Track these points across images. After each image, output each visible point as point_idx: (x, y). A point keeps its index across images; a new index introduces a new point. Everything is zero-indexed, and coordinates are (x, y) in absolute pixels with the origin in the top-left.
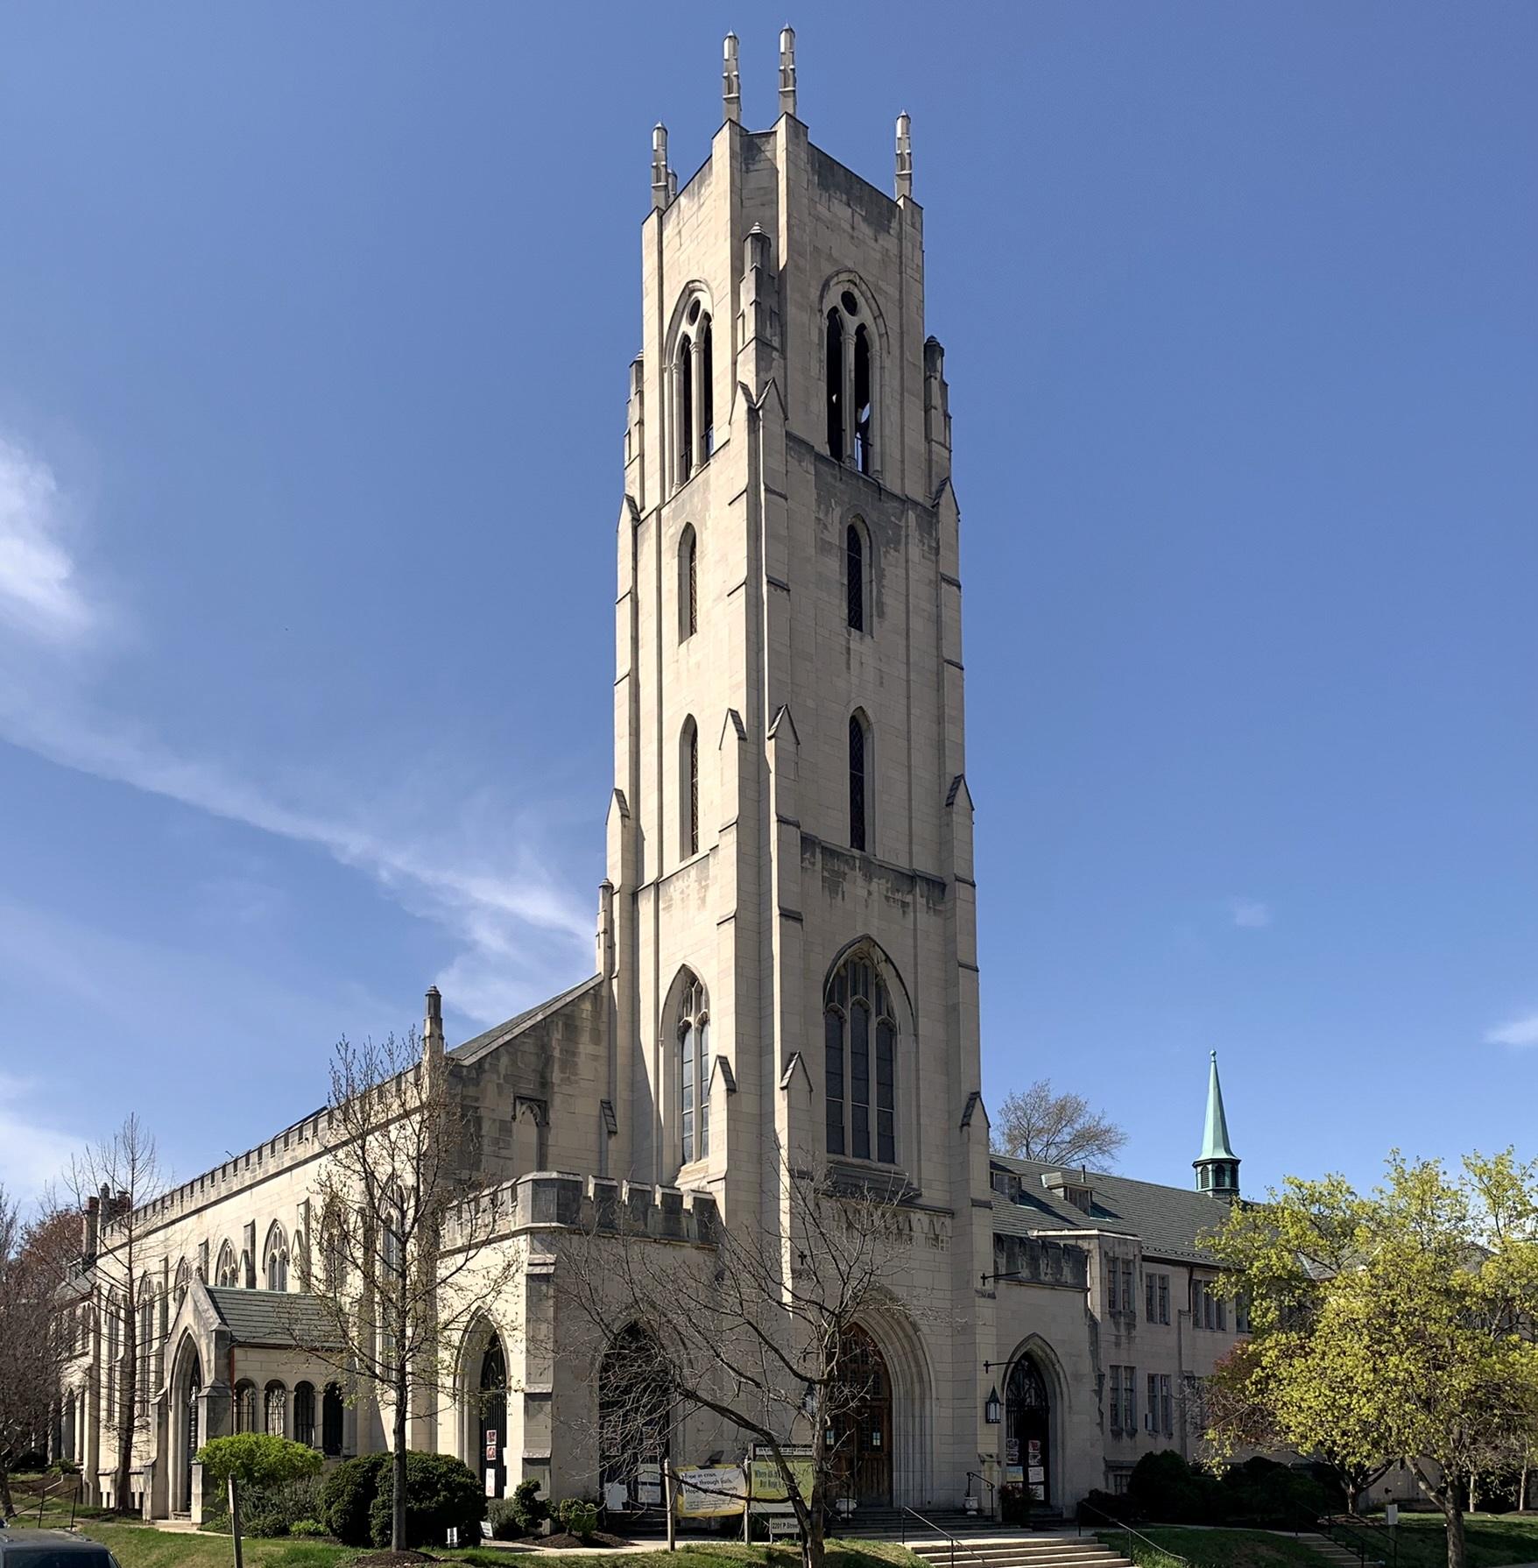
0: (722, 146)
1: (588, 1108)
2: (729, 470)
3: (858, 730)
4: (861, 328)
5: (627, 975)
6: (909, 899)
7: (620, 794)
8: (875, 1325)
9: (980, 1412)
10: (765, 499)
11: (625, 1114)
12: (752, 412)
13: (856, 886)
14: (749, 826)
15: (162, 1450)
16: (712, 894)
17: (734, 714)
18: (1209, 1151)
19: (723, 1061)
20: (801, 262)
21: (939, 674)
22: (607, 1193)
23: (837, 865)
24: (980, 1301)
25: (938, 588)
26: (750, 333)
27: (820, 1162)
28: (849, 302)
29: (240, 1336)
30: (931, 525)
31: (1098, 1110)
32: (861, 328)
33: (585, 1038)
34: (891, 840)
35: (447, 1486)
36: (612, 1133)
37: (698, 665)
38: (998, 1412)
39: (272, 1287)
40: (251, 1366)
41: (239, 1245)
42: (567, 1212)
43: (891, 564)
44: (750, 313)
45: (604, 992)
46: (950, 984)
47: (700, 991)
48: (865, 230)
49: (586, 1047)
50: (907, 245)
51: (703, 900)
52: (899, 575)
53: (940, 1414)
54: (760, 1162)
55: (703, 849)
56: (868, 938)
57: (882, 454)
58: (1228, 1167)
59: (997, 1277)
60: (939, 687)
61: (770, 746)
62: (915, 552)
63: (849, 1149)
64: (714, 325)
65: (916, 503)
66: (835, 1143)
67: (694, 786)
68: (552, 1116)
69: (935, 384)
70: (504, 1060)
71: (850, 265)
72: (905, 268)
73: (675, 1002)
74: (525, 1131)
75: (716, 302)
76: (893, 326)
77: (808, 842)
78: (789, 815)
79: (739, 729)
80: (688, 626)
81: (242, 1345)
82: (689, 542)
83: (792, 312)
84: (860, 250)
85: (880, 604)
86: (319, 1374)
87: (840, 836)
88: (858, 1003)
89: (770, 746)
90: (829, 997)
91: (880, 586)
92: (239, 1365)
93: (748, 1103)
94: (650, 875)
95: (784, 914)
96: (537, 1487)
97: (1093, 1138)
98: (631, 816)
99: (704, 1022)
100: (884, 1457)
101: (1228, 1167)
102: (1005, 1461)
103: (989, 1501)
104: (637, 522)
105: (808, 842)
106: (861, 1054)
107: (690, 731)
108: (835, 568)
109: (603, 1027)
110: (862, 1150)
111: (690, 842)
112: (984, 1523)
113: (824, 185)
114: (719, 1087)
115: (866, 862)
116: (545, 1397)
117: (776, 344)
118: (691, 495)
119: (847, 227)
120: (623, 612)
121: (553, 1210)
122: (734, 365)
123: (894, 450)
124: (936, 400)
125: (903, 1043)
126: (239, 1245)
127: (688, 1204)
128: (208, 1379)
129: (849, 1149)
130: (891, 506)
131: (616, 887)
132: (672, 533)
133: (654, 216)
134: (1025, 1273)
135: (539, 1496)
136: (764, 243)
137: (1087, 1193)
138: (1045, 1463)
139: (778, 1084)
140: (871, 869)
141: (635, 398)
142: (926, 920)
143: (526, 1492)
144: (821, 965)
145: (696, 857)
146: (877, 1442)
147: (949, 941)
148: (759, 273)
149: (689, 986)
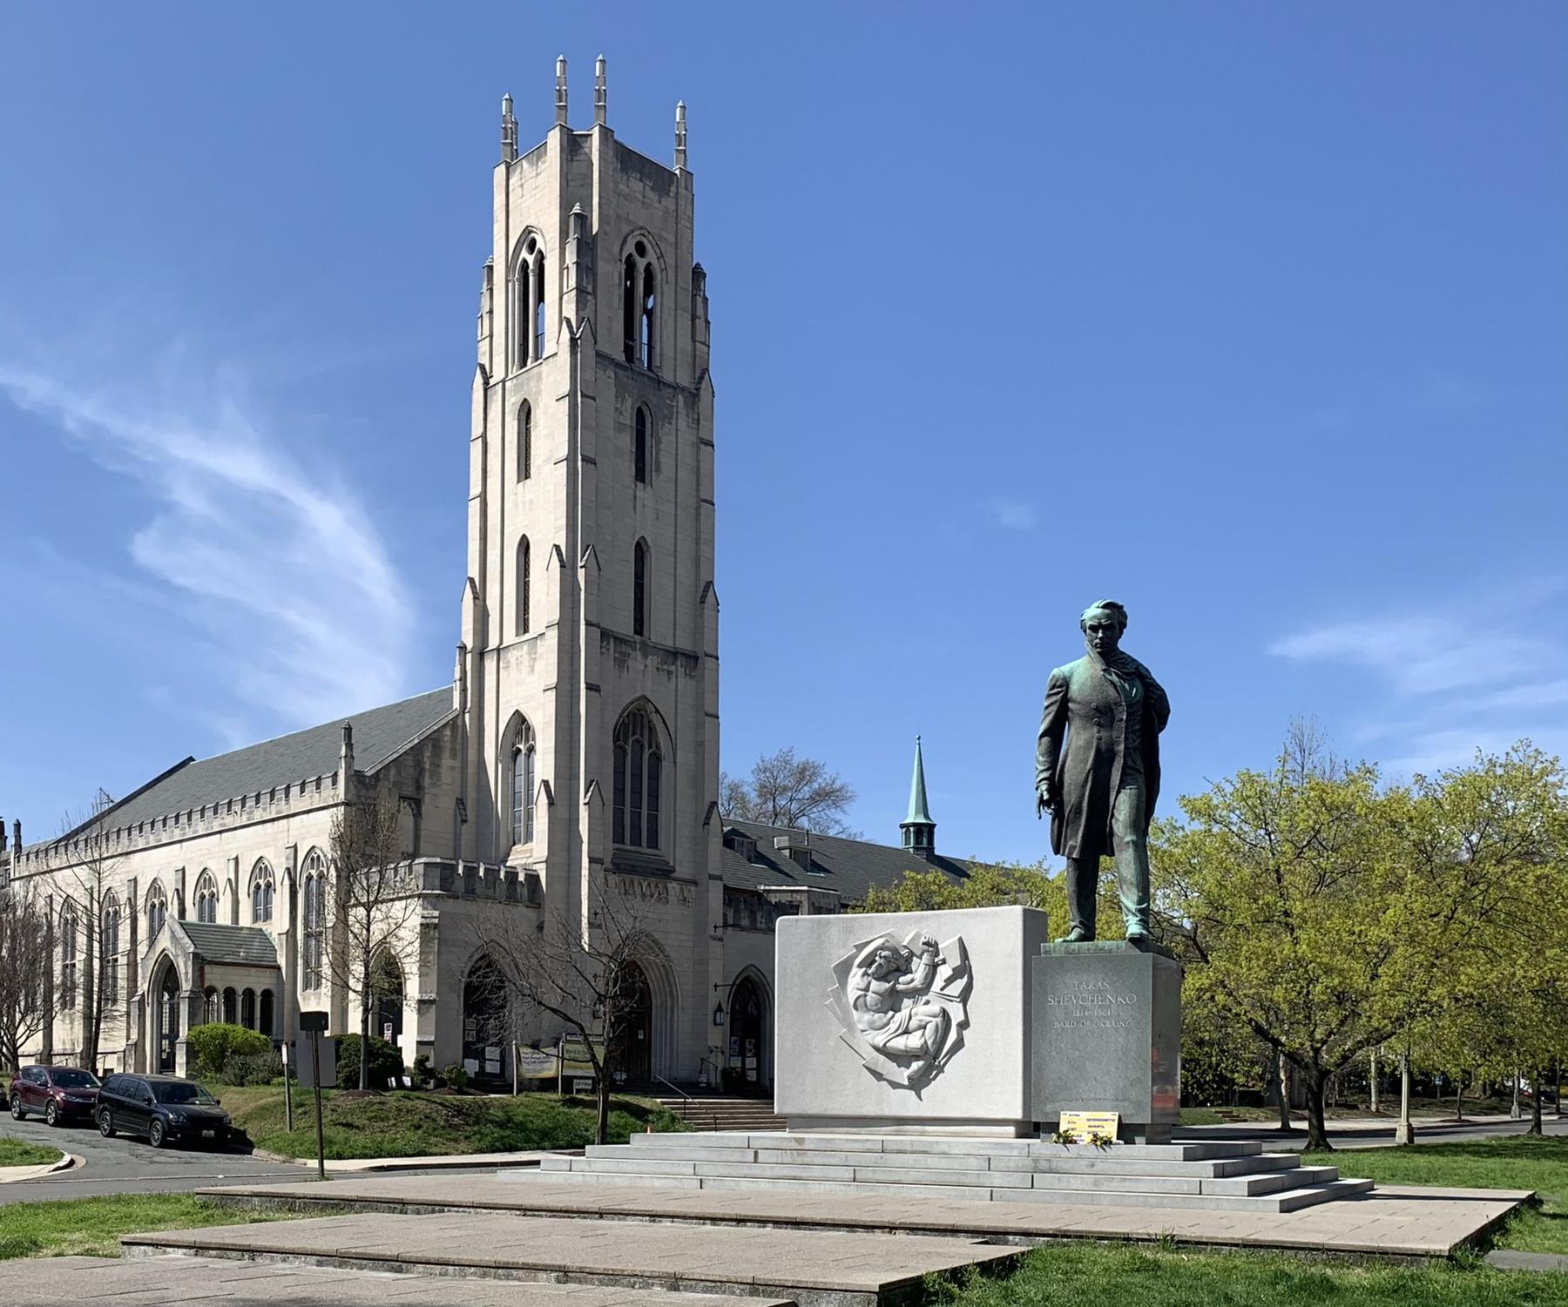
0: (554, 139)
1: (448, 803)
2: (556, 341)
3: (641, 550)
4: (649, 264)
5: (475, 710)
6: (673, 668)
7: (472, 580)
8: (648, 959)
9: (710, 1017)
10: (581, 398)
11: (471, 804)
12: (573, 341)
13: (637, 662)
14: (567, 625)
15: (142, 1034)
16: (539, 665)
17: (557, 547)
18: (912, 817)
19: (546, 783)
20: (608, 229)
21: (698, 509)
22: (471, 871)
23: (624, 648)
24: (713, 943)
25: (698, 449)
26: (573, 283)
27: (608, 849)
28: (641, 249)
29: (208, 956)
30: (694, 403)
31: (833, 771)
32: (649, 264)
33: (446, 754)
34: (660, 630)
35: (383, 1055)
36: (464, 821)
37: (531, 501)
38: (724, 1018)
39: (201, 918)
40: (217, 978)
41: (169, 885)
42: (449, 885)
43: (666, 434)
44: (573, 269)
45: (459, 722)
46: (699, 727)
47: (528, 728)
48: (653, 196)
49: (446, 761)
50: (682, 203)
51: (532, 668)
52: (671, 440)
53: (684, 1020)
54: (569, 851)
55: (532, 634)
56: (644, 697)
57: (661, 355)
58: (925, 830)
59: (726, 925)
60: (697, 518)
61: (581, 573)
62: (682, 425)
63: (627, 841)
64: (546, 262)
65: (683, 389)
66: (618, 837)
67: (526, 584)
68: (424, 808)
69: (699, 299)
70: (393, 772)
71: (641, 224)
72: (681, 221)
73: (511, 734)
74: (406, 820)
75: (549, 241)
76: (670, 260)
77: (605, 635)
78: (593, 620)
79: (561, 560)
80: (524, 472)
81: (210, 963)
82: (525, 412)
83: (602, 267)
84: (647, 211)
85: (658, 463)
86: (259, 982)
87: (625, 627)
88: (637, 741)
89: (581, 573)
90: (616, 738)
91: (658, 450)
92: (207, 976)
93: (562, 812)
94: (493, 642)
95: (589, 687)
96: (427, 1059)
97: (829, 796)
98: (480, 598)
99: (531, 749)
100: (646, 1045)
101: (925, 830)
102: (727, 1052)
103: (716, 1079)
104: (486, 383)
105: (605, 635)
106: (637, 776)
107: (524, 546)
108: (627, 441)
109: (458, 747)
110: (636, 841)
111: (523, 625)
112: (710, 1091)
113: (624, 170)
114: (542, 801)
115: (644, 645)
116: (432, 1002)
117: (590, 289)
118: (528, 380)
119: (639, 196)
120: (476, 449)
121: (437, 882)
122: (559, 304)
123: (669, 352)
124: (700, 312)
125: (666, 766)
126: (169, 885)
127: (521, 878)
128: (186, 986)
129: (627, 841)
130: (667, 392)
131: (469, 646)
132: (513, 401)
133: (503, 167)
134: (745, 922)
135: (429, 1064)
136: (583, 219)
137: (807, 853)
138: (757, 1055)
139: (582, 801)
140: (647, 649)
141: (487, 294)
142: (684, 683)
143: (420, 1062)
144: (612, 719)
145: (527, 636)
146: (641, 1037)
147: (699, 696)
148: (579, 241)
149: (520, 725)
